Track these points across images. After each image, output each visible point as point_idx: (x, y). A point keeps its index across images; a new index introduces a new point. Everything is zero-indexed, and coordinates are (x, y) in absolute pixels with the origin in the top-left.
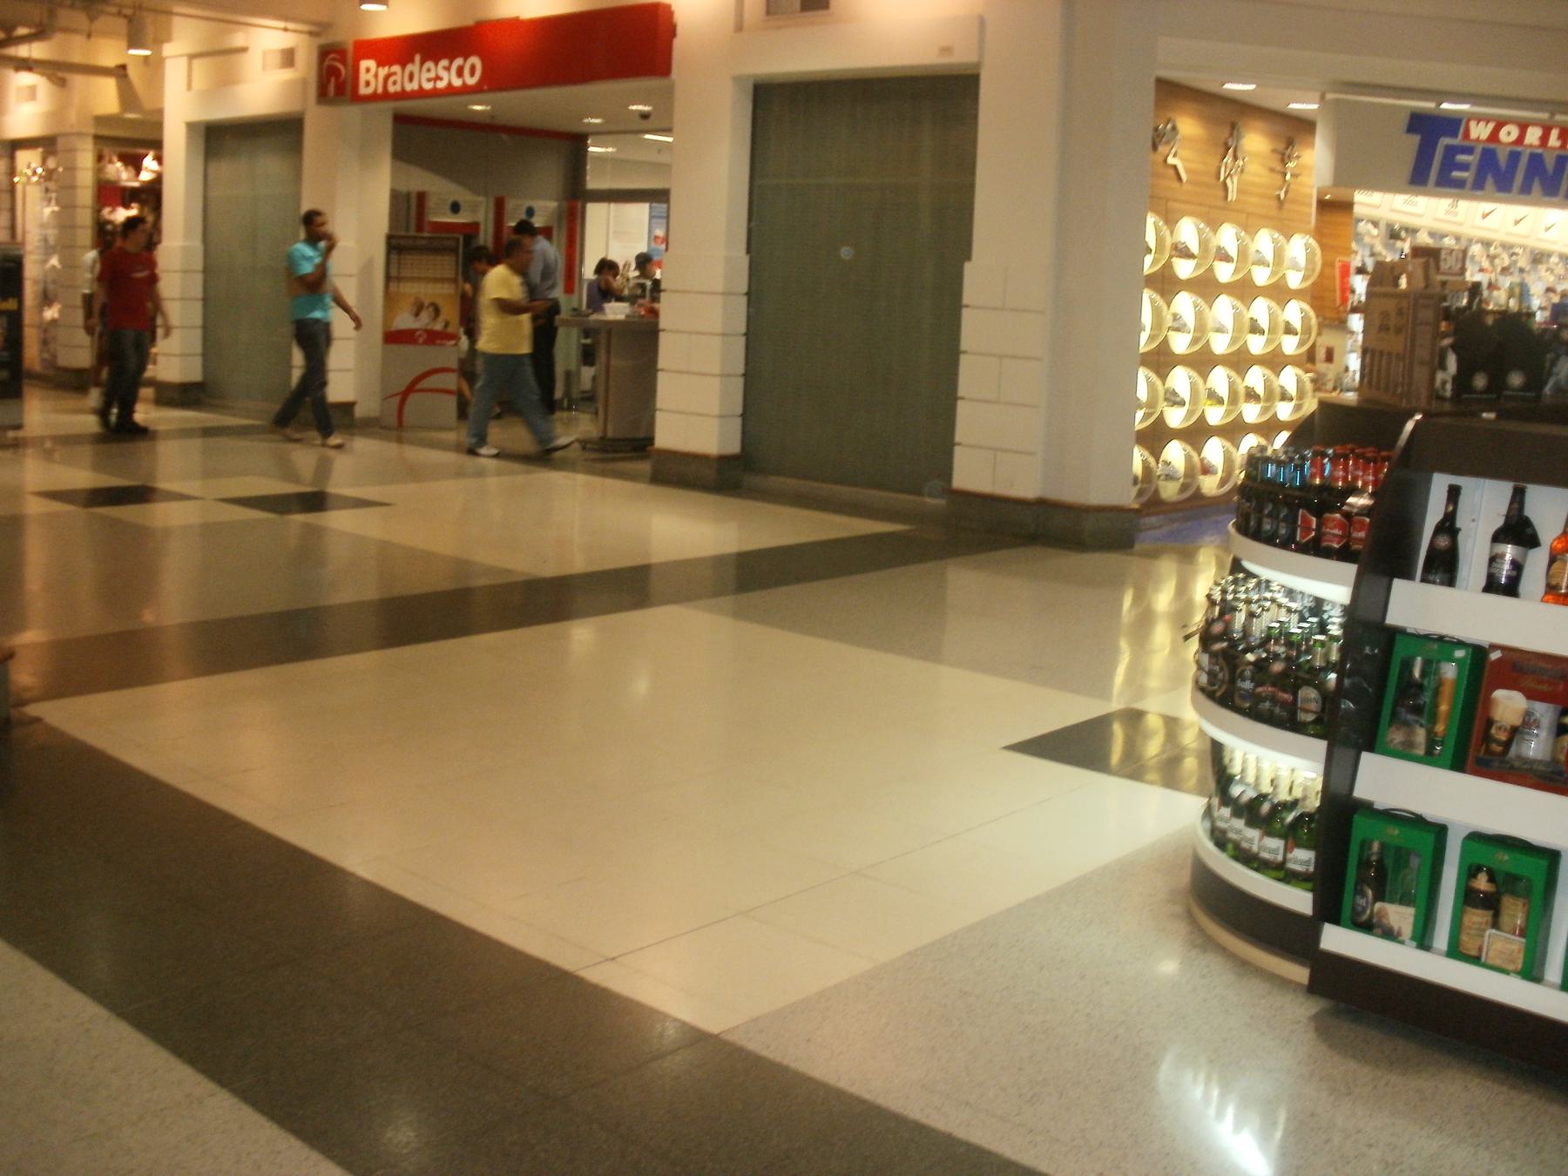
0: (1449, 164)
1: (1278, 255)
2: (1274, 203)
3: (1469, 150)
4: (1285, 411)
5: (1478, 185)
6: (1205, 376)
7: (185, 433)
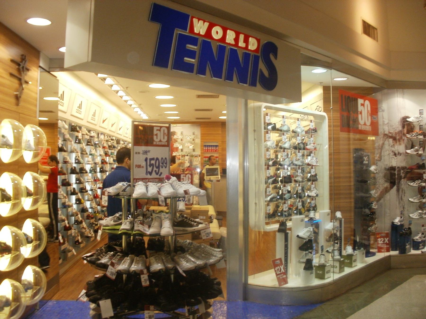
0: (182, 52)
1: (18, 138)
2: (13, 100)
3: (194, 41)
4: (27, 251)
5: (202, 71)
6: (20, 227)
7: (350, 169)
